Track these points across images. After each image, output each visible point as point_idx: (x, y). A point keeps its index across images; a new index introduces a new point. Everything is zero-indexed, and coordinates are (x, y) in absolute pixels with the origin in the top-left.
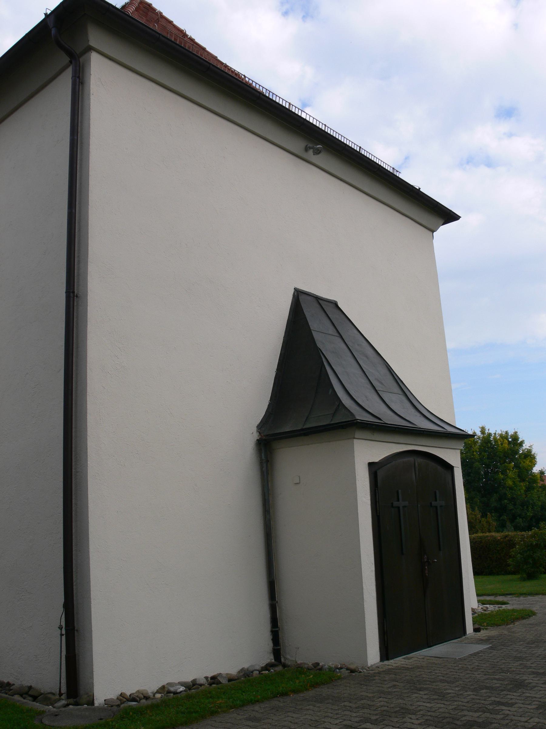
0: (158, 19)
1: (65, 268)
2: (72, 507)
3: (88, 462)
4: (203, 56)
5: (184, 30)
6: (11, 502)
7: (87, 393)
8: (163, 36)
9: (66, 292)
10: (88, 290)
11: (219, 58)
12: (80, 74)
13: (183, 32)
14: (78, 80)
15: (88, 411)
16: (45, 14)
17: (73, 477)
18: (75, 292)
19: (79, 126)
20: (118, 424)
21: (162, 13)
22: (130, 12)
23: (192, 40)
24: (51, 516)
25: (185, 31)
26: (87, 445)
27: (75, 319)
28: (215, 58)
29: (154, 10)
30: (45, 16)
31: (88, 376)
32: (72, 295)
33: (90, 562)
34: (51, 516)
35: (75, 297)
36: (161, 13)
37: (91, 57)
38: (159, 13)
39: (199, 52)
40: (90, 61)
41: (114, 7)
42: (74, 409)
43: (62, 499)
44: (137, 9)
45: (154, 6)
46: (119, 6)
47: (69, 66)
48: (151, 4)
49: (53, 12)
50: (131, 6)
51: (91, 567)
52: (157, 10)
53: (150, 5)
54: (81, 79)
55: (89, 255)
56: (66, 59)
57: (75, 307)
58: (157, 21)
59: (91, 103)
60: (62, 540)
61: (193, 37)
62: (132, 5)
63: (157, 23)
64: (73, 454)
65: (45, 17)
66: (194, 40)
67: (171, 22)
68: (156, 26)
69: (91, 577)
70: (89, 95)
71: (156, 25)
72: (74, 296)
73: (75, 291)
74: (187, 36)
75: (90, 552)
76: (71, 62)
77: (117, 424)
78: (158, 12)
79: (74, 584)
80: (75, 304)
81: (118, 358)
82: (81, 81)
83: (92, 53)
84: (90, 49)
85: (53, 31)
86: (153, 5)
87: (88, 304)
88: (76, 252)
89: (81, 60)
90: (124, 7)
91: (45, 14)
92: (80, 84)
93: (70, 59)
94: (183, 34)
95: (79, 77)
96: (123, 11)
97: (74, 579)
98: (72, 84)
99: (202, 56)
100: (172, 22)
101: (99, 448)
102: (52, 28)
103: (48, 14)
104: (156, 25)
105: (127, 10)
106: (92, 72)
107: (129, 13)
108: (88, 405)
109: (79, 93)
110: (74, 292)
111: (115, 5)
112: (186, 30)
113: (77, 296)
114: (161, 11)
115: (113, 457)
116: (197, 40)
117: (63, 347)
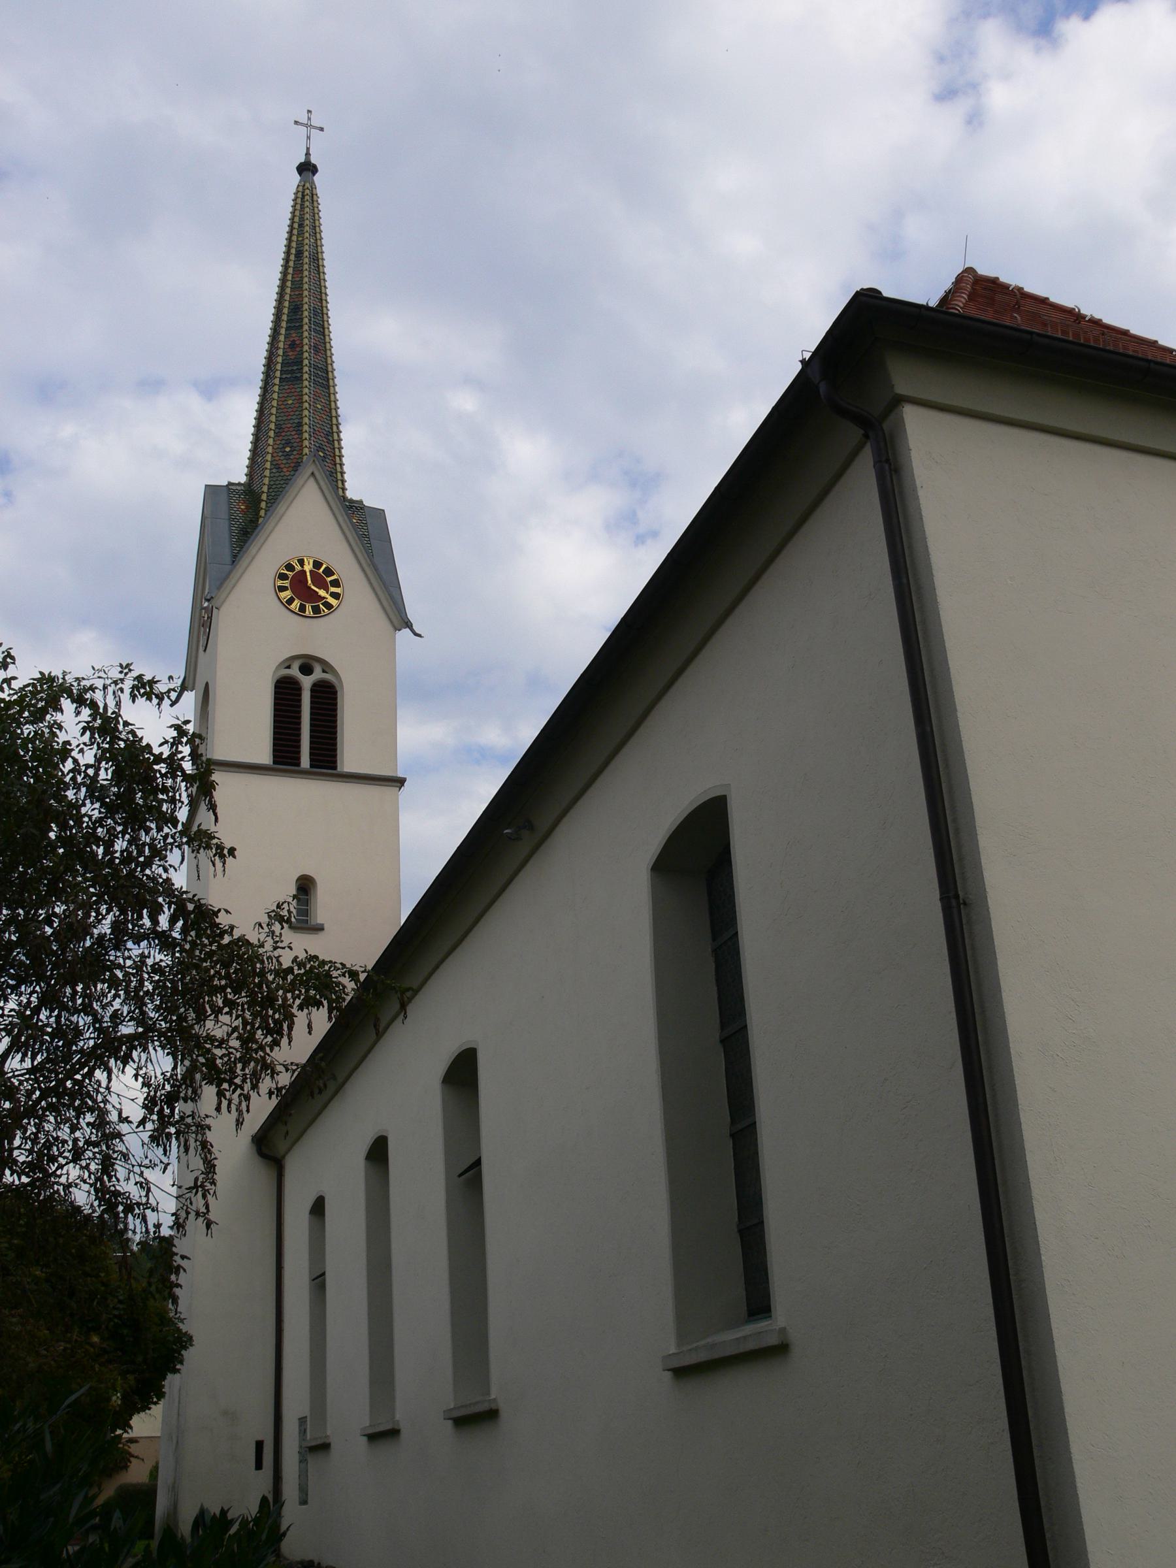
0: (1017, 303)
1: (930, 849)
2: (1019, 1361)
3: (1043, 1258)
4: (1130, 347)
5: (1074, 309)
6: (886, 1356)
7: (1018, 1105)
8: (1039, 335)
9: (941, 899)
10: (986, 887)
11: (1162, 342)
12: (888, 453)
13: (997, 282)
14: (887, 467)
15: (1027, 1146)
16: (801, 361)
17: (1014, 1292)
18: (960, 896)
19: (906, 555)
20: (1095, 1165)
21: (1023, 288)
22: (959, 306)
23: (1096, 323)
24: (977, 1382)
25: (1077, 310)
26: (1035, 1220)
27: (969, 953)
28: (1153, 344)
29: (1005, 287)
30: (802, 364)
31: (1015, 1070)
32: (954, 903)
33: (1078, 1485)
34: (977, 1382)
35: (962, 906)
36: (1020, 289)
37: (905, 416)
38: (1016, 291)
39: (1121, 344)
40: (904, 422)
41: (926, 308)
42: (995, 1144)
43: (996, 1344)
44: (972, 297)
45: (1004, 279)
46: (933, 303)
47: (865, 443)
48: (997, 278)
49: (815, 354)
50: (959, 294)
51: (1080, 1495)
52: (1011, 285)
53: (994, 282)
54: (892, 464)
55: (975, 814)
56: (856, 433)
57: (964, 926)
58: (1017, 307)
59: (921, 506)
60: (1007, 1436)
61: (1097, 316)
62: (959, 292)
63: (1018, 311)
64: (1007, 1242)
65: (802, 367)
66: (1101, 320)
67: (1044, 301)
68: (1016, 317)
69: (1084, 1519)
70: (915, 490)
71: (1015, 315)
72: (959, 905)
73: (960, 893)
74: (1083, 317)
75: (1074, 1461)
76: (866, 436)
77: (1094, 1167)
78: (1014, 290)
79: (1048, 1535)
80: (964, 921)
81: (1074, 1021)
82: (892, 467)
83: (903, 407)
84: (899, 401)
85: (823, 388)
86: (1001, 280)
87: (992, 916)
88: (948, 812)
89: (885, 426)
90: (944, 300)
91: (801, 361)
92: (893, 473)
93: (862, 432)
94: (1073, 316)
95: (888, 461)
96: (944, 309)
97: (1046, 1526)
98: (878, 480)
99: (1128, 349)
100: (1128, 331)
101: (1063, 1224)
102: (819, 383)
103: (807, 359)
104: (1015, 315)
105: (953, 304)
106: (911, 446)
107: (959, 310)
108: (1024, 1133)
109: (894, 491)
110: (957, 896)
111: (925, 304)
112: (1078, 306)
113: (965, 904)
114: (1021, 286)
115: (1096, 1240)
116: (1107, 320)
117: (954, 1015)
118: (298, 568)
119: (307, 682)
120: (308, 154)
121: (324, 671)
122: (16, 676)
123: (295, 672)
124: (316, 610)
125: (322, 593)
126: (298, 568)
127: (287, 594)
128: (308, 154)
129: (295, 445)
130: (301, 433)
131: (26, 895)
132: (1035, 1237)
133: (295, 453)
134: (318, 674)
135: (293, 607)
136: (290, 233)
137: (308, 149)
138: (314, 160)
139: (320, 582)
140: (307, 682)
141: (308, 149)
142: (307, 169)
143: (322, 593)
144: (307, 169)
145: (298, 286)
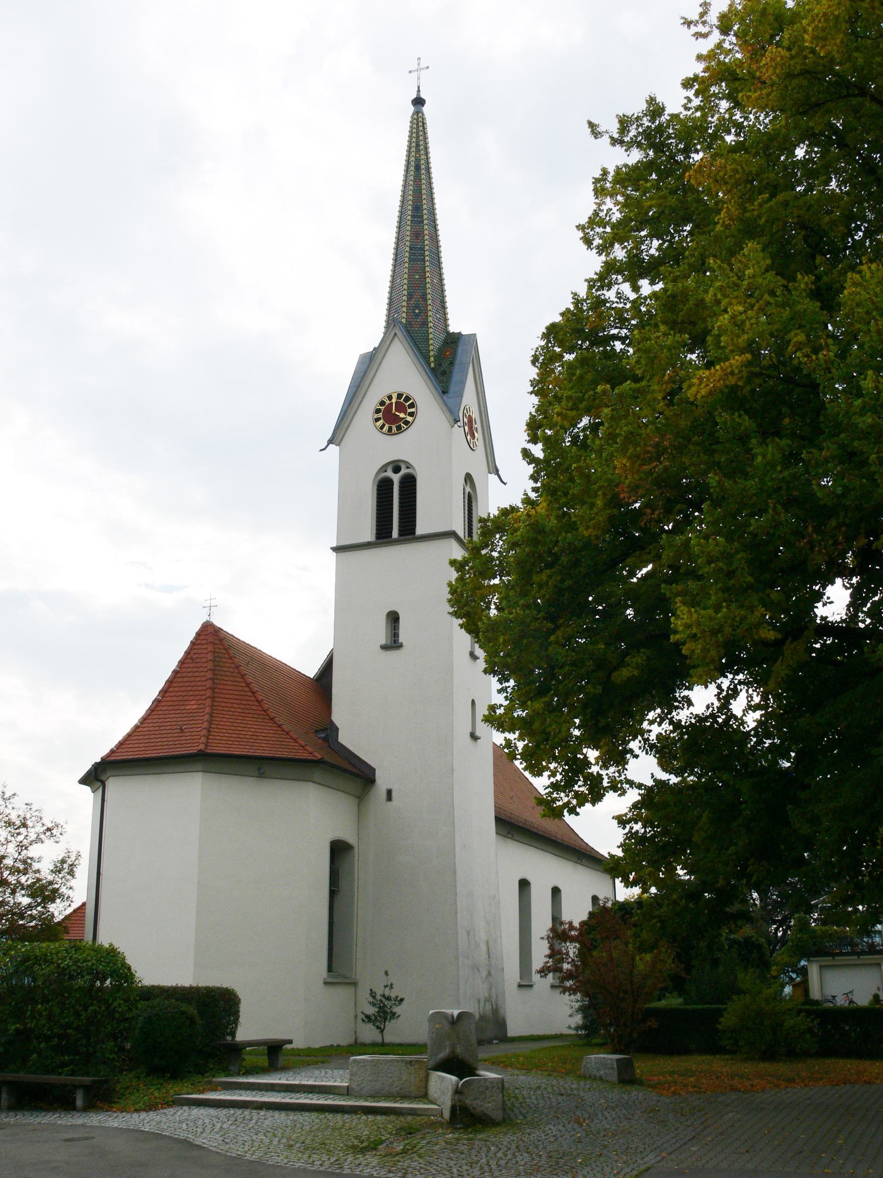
118: (388, 402)
119: (396, 478)
120: (419, 91)
121: (408, 468)
122: (520, 456)
123: (390, 474)
124: (399, 428)
125: (402, 415)
126: (388, 402)
127: (381, 422)
128: (419, 91)
129: (422, 308)
130: (426, 300)
131: (637, 534)
132: (295, 784)
133: (422, 314)
134: (404, 471)
135: (384, 430)
136: (409, 151)
137: (419, 87)
138: (423, 96)
139: (400, 407)
140: (396, 478)
141: (419, 87)
142: (419, 102)
143: (402, 415)
144: (419, 102)
145: (418, 192)
